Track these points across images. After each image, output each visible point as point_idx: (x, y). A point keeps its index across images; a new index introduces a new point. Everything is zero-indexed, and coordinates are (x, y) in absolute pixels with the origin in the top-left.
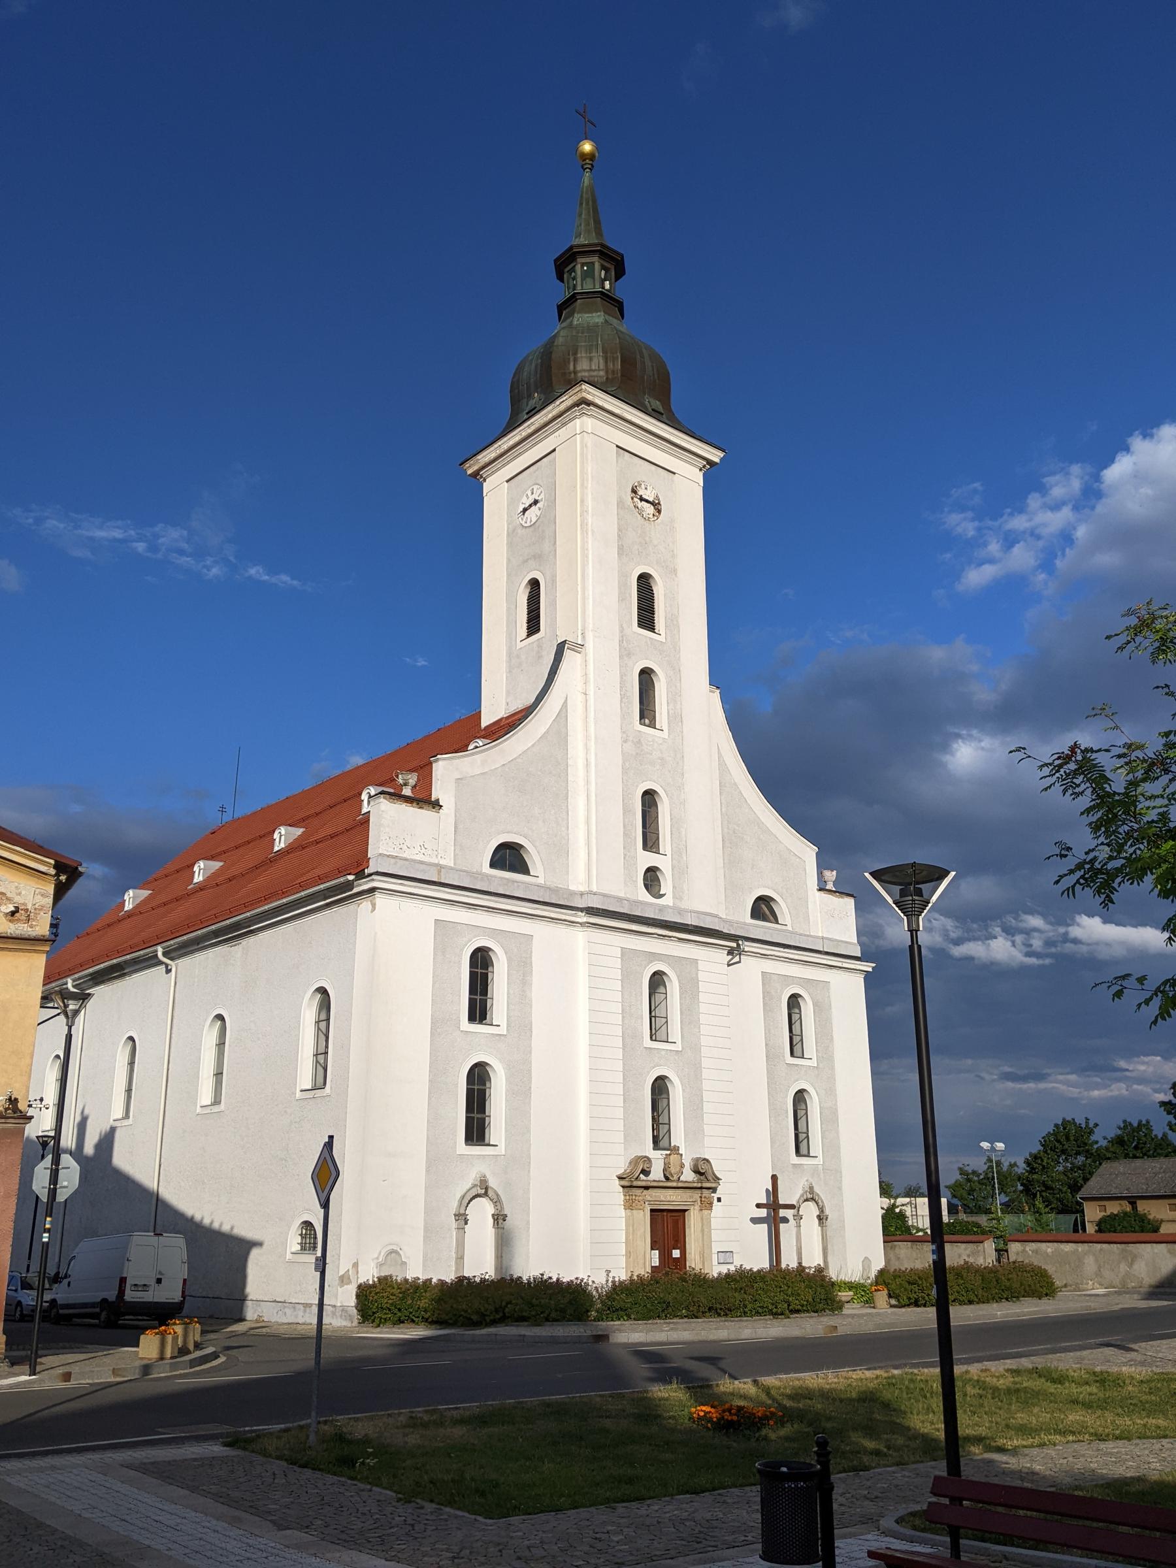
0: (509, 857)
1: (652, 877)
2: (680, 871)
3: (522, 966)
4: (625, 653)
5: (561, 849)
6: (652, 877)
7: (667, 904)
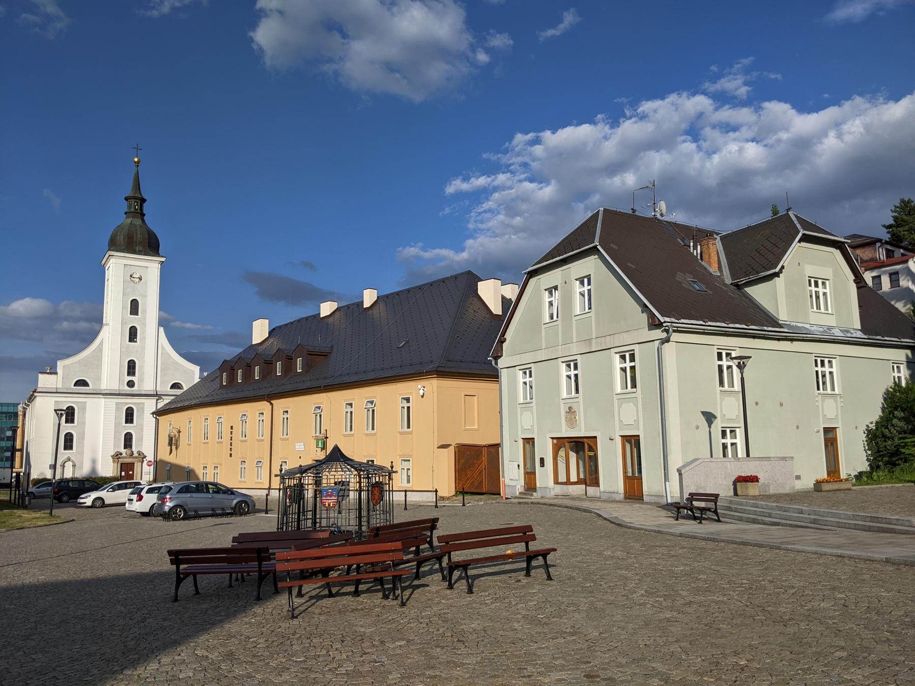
0: (81, 383)
2: (141, 380)
3: (83, 407)
4: (123, 323)
5: (99, 379)
6: (131, 384)
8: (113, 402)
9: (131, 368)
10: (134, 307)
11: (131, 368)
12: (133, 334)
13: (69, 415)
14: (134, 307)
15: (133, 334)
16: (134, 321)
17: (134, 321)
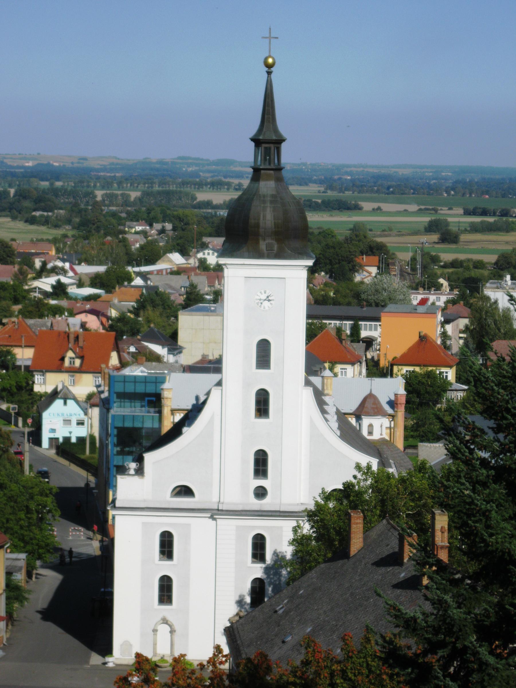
0: (185, 491)
1: (261, 493)
7: (266, 503)
8: (228, 525)
9: (261, 463)
10: (263, 354)
11: (261, 463)
12: (262, 404)
13: (166, 546)
14: (263, 354)
15: (262, 404)
16: (263, 379)
17: (263, 379)
